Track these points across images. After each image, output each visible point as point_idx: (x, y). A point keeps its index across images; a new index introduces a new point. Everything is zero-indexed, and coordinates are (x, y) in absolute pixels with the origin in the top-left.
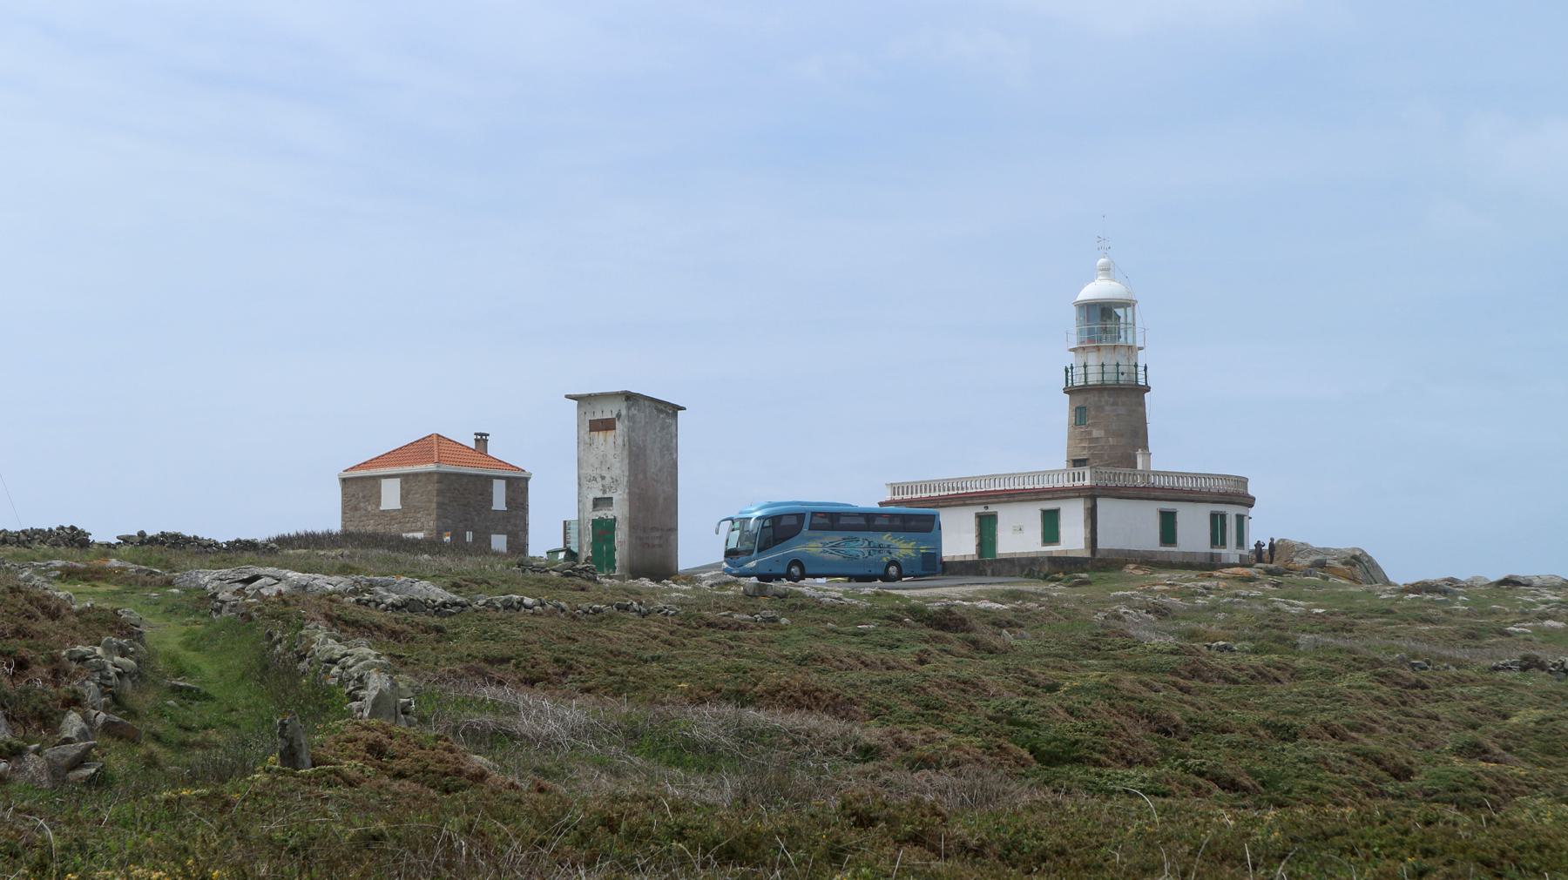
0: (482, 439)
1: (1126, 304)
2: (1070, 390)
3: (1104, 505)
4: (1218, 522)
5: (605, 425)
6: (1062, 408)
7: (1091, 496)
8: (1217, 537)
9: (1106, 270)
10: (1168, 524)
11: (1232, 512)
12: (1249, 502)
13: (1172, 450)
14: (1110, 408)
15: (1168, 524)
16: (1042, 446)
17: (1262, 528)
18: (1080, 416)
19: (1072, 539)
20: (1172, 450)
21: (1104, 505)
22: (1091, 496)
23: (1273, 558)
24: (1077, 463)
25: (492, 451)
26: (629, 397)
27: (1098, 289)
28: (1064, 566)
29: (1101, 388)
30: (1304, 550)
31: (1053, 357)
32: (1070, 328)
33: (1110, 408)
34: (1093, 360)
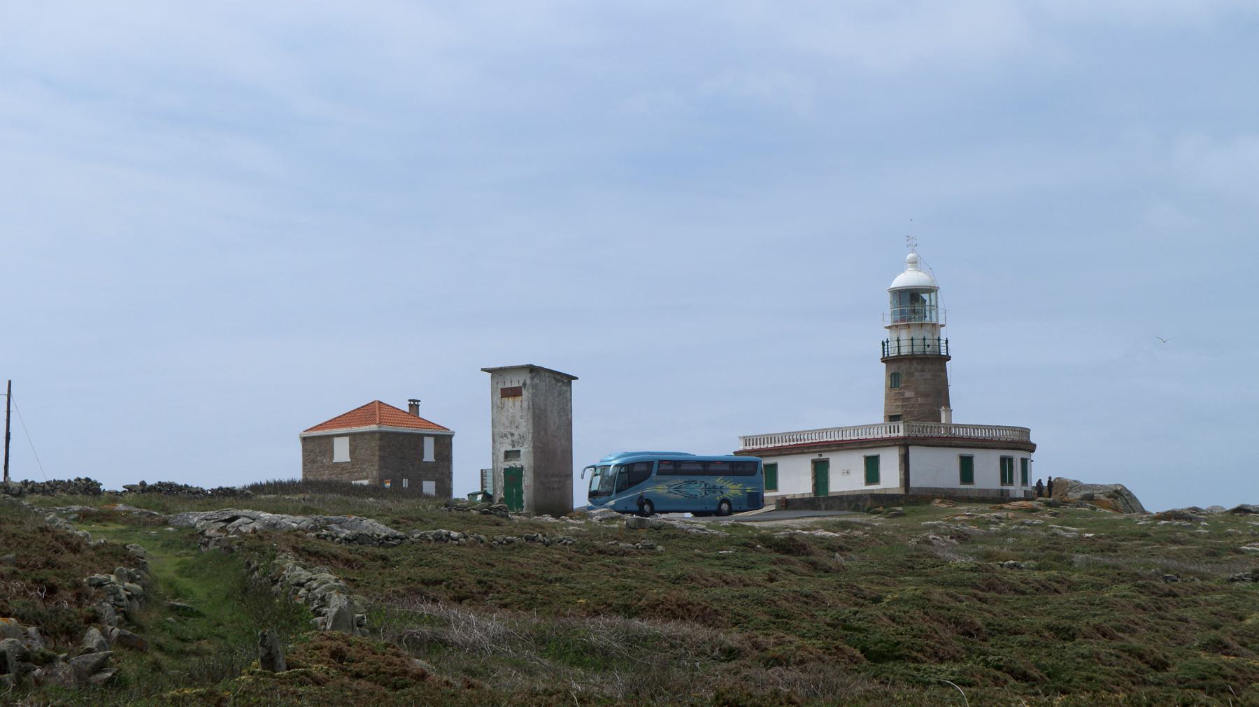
0: (414, 405)
1: (931, 290)
2: (886, 360)
3: (914, 452)
4: (1006, 464)
5: (514, 393)
6: (879, 375)
7: (904, 445)
8: (1006, 476)
9: (914, 262)
10: (967, 466)
11: (1017, 456)
12: (1031, 448)
13: (969, 406)
14: (918, 374)
15: (967, 466)
16: (863, 404)
17: (1041, 470)
18: (894, 380)
19: (890, 479)
20: (969, 406)
21: (914, 452)
22: (904, 445)
23: (1052, 492)
24: (892, 418)
25: (423, 414)
26: (532, 370)
27: (908, 278)
28: (883, 501)
29: (911, 358)
30: (1076, 486)
31: (873, 334)
32: (885, 310)
33: (918, 374)
34: (904, 335)
